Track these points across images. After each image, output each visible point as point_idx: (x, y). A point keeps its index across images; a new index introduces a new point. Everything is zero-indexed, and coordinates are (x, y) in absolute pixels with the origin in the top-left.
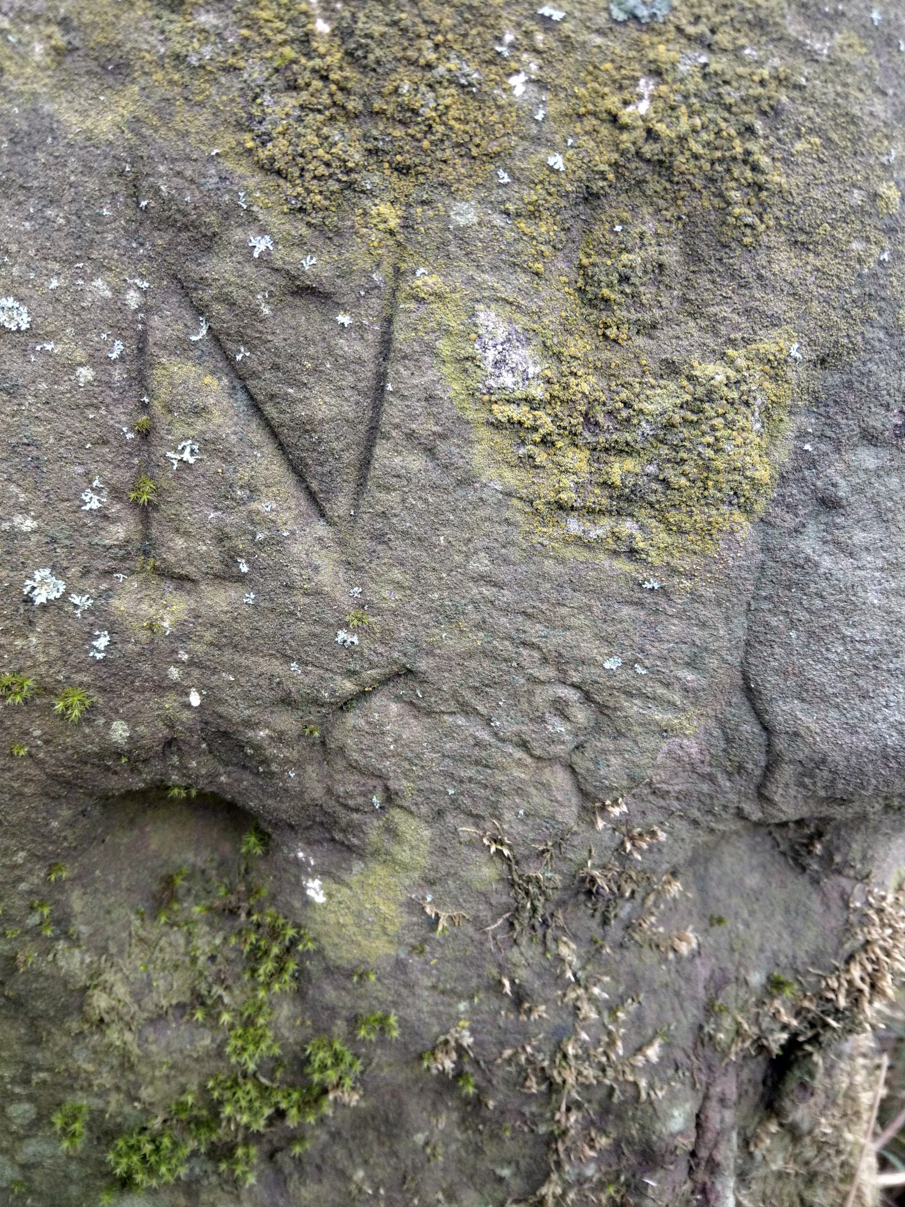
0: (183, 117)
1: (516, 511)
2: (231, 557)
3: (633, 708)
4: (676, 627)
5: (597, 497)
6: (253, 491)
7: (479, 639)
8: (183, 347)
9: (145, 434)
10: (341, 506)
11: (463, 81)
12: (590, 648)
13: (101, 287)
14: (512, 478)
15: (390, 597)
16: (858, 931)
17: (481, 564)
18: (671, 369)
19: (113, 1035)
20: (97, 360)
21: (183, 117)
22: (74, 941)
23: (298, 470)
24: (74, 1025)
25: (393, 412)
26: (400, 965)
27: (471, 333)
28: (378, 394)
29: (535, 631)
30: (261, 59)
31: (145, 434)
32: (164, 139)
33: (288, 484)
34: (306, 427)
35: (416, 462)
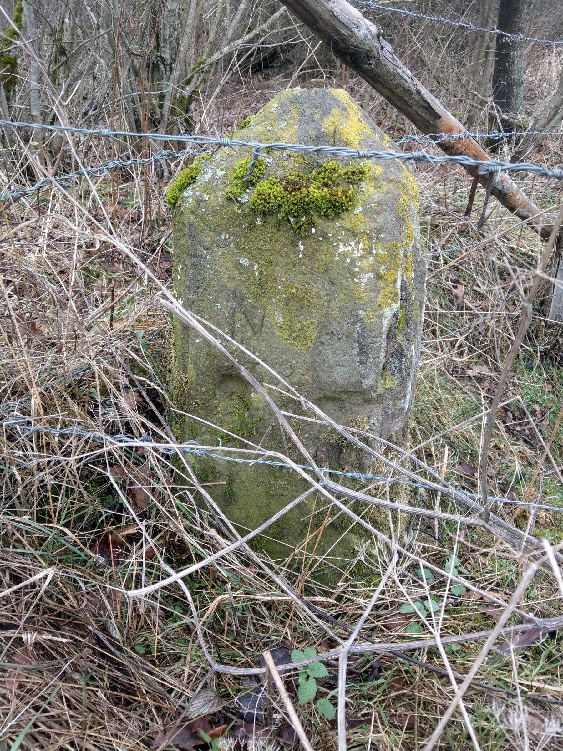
0: (241, 286)
1: (280, 338)
2: (243, 340)
3: (298, 370)
4: (303, 358)
5: (291, 338)
6: (247, 332)
7: (275, 356)
8: (239, 312)
9: (234, 322)
10: (258, 335)
11: (413, 495)
12: (291, 360)
13: (230, 304)
14: (280, 334)
15: (264, 349)
16: (281, 75)
17: (276, 345)
18: (300, 322)
19: (220, 415)
20: (229, 313)
21: (241, 286)
22: (216, 398)
23: (253, 329)
24: (214, 413)
25: (265, 323)
26: (264, 408)
27: (274, 314)
28: (263, 321)
29: (283, 356)
30: (177, 198)
31: (234, 322)
32: (239, 288)
33: (251, 331)
34: (254, 324)
35: (267, 330)
